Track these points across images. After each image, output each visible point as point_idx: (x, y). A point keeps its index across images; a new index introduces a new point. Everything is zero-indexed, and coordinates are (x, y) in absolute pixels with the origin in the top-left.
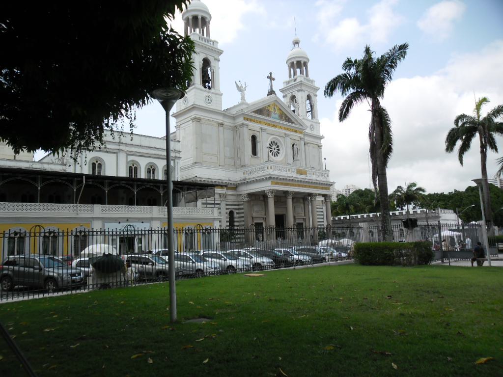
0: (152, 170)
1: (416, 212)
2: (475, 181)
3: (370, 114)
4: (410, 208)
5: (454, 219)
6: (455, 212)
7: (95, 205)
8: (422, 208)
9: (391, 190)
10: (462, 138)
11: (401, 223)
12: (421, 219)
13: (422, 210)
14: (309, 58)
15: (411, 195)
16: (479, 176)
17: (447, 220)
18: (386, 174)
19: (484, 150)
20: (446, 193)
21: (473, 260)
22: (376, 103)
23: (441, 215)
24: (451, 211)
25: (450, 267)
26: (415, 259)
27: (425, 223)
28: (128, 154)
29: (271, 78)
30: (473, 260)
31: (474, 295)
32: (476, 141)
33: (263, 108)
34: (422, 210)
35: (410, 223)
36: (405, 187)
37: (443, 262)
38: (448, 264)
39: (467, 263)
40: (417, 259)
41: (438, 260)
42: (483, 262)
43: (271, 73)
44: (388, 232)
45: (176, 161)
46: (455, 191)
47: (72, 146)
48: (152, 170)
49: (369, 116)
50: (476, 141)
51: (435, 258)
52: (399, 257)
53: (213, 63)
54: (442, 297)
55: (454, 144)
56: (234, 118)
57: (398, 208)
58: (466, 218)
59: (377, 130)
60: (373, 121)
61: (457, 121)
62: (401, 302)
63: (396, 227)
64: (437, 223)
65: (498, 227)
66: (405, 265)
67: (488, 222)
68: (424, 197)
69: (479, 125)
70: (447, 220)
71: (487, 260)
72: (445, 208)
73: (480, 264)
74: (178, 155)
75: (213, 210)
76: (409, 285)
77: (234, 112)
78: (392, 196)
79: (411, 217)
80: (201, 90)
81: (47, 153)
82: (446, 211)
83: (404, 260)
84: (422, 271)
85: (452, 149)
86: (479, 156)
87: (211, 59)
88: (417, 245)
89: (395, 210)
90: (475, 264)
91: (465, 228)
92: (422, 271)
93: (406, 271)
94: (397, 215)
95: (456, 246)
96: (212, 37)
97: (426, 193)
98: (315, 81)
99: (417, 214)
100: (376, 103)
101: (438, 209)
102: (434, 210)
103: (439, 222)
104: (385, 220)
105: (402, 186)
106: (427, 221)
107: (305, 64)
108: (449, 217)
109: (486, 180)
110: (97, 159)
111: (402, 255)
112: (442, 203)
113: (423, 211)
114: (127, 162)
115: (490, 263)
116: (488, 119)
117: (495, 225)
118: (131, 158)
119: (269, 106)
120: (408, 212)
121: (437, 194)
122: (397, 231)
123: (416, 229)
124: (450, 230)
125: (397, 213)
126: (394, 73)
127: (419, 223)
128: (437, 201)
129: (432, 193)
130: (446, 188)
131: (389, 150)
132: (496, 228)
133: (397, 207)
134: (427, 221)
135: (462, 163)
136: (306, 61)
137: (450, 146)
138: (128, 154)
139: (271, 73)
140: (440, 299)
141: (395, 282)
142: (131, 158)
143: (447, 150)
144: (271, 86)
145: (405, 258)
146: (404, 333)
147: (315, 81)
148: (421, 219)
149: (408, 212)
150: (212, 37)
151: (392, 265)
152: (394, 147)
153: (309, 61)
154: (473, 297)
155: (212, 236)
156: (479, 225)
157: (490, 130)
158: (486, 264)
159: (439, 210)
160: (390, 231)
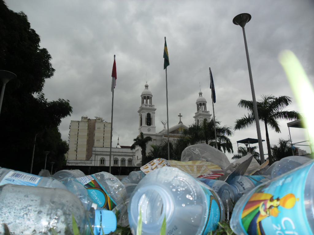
0: (123, 161)
14: (152, 95)
19: (151, 221)
28: (114, 155)
29: (180, 116)
33: (175, 130)
43: (180, 114)
45: (133, 157)
48: (123, 161)
53: (152, 115)
56: (161, 136)
74: (134, 154)
77: (160, 134)
80: (146, 127)
87: (151, 113)
96: (207, 110)
98: (209, 112)
107: (151, 98)
110: (103, 158)
114: (114, 159)
118: (115, 157)
119: (178, 129)
136: (151, 96)
138: (114, 155)
139: (180, 114)
142: (115, 157)
144: (180, 120)
147: (209, 112)
150: (207, 110)
153: (152, 96)
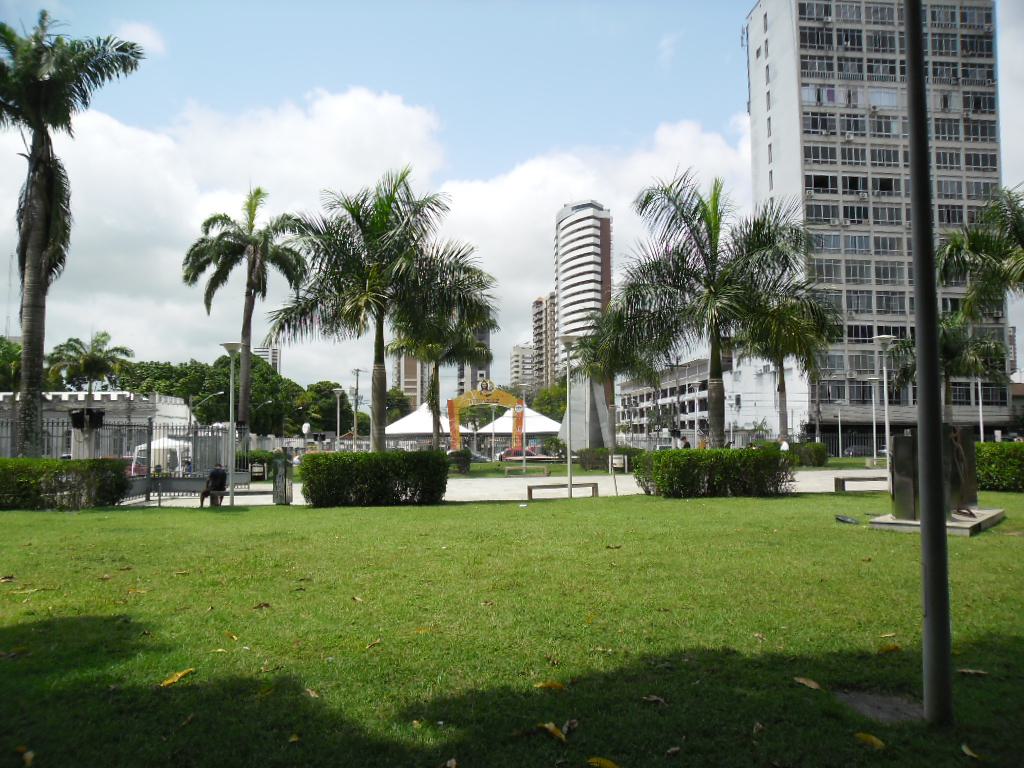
1: (108, 396)
2: (227, 346)
3: (24, 167)
4: (98, 391)
5: (184, 415)
6: (187, 402)
7: (370, 383)
8: (122, 390)
9: (48, 349)
10: (216, 262)
11: (67, 419)
12: (115, 412)
13: (120, 393)
15: (94, 365)
16: (237, 338)
17: (169, 417)
18: (44, 307)
20: (175, 364)
21: (204, 496)
22: (42, 143)
23: (159, 406)
24: (180, 401)
25: (232, 508)
26: (89, 494)
27: (124, 421)
30: (204, 496)
31: (189, 560)
32: (240, 272)
34: (120, 393)
35: (89, 419)
36: (87, 339)
37: (148, 499)
38: (157, 505)
39: (194, 501)
40: (93, 493)
41: (138, 494)
42: (222, 498)
44: (34, 435)
46: (194, 362)
47: (828, 312)
49: (22, 171)
50: (240, 272)
51: (132, 492)
52: (53, 491)
54: (128, 569)
55: (202, 268)
57: (69, 386)
58: (209, 414)
59: (37, 204)
60: (31, 183)
61: (208, 224)
62: (33, 585)
63: (55, 426)
64: (145, 422)
65: (258, 435)
66: (62, 508)
67: (240, 424)
68: (127, 369)
69: (249, 243)
70: (169, 417)
71: (227, 494)
72: (169, 394)
73: (215, 504)
75: (575, 410)
76: (62, 549)
78: (52, 360)
79: (95, 407)
81: (618, 278)
82: (169, 398)
83: (62, 497)
84: (99, 520)
85: (195, 279)
86: (242, 300)
88: (98, 466)
89: (62, 389)
90: (207, 502)
91: (199, 434)
92: (99, 520)
93: (64, 521)
94: (65, 401)
95: (177, 469)
97: (134, 360)
99: (110, 401)
100: (42, 143)
101: (155, 395)
102: (147, 396)
103: (150, 419)
104: (32, 409)
105: (82, 340)
106: (129, 418)
108: (175, 412)
109: (247, 347)
111: (62, 487)
112: (162, 383)
113: (123, 396)
115: (232, 501)
116: (266, 236)
117: (252, 432)
120: (90, 397)
121: (157, 364)
122: (60, 433)
123: (103, 432)
124: (170, 437)
125: (65, 396)
126: (97, 94)
127: (107, 420)
128: (156, 379)
129: (147, 359)
130: (176, 355)
131: (58, 259)
132: (253, 436)
133: (68, 383)
134: (129, 418)
135: (209, 313)
137: (191, 278)
140: (122, 573)
141: (30, 544)
143: (186, 278)
145: (65, 493)
146: (22, 653)
148: (115, 412)
149: (90, 397)
151: (33, 510)
152: (71, 255)
154: (186, 562)
155: (161, 457)
156: (224, 430)
157: (265, 257)
158: (226, 501)
159: (157, 396)
160: (37, 435)
